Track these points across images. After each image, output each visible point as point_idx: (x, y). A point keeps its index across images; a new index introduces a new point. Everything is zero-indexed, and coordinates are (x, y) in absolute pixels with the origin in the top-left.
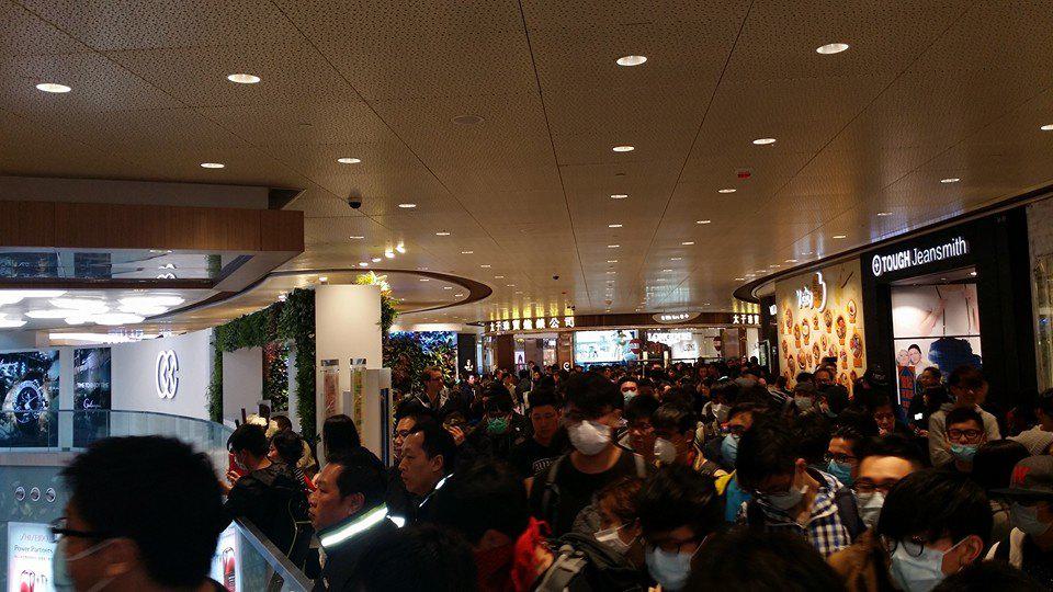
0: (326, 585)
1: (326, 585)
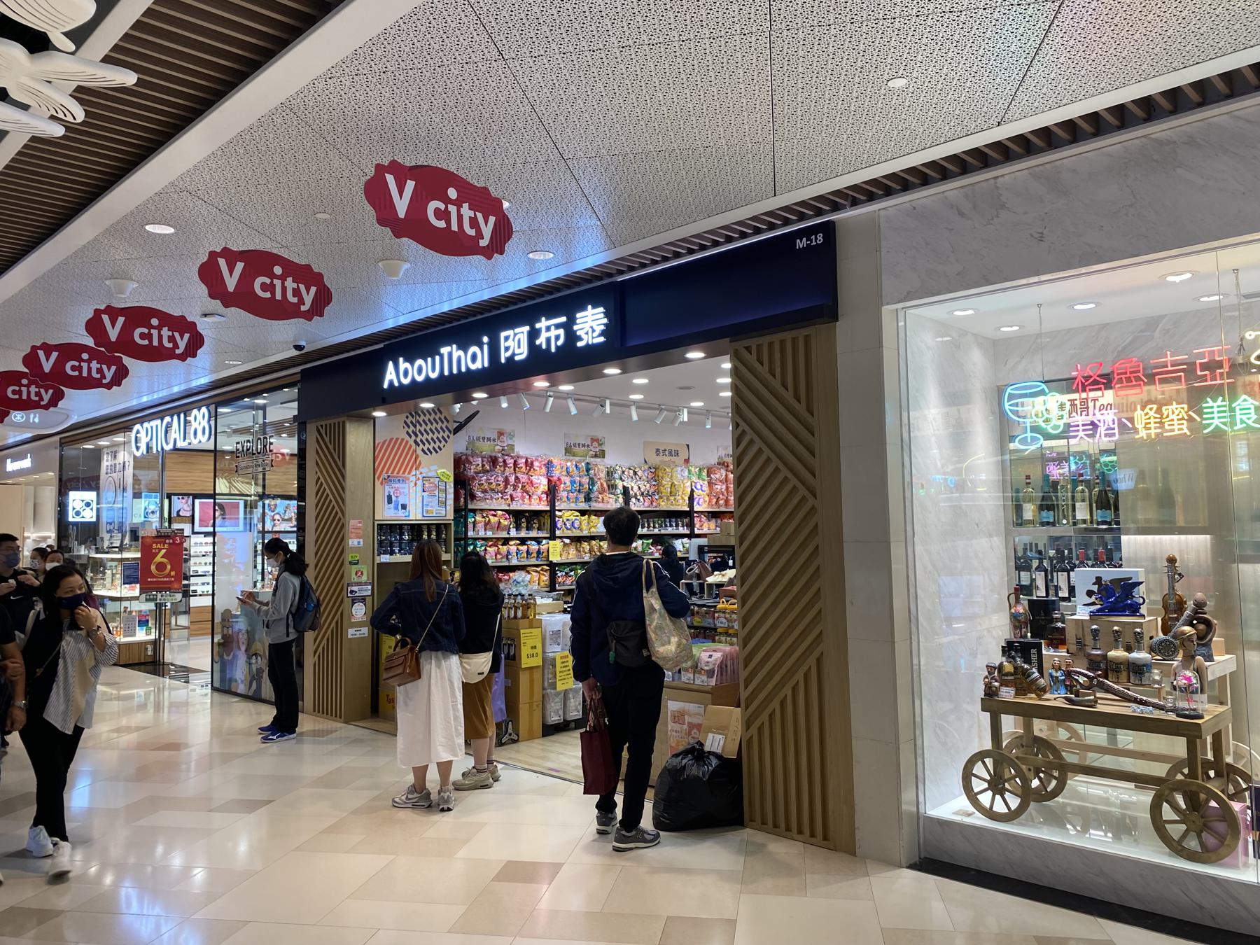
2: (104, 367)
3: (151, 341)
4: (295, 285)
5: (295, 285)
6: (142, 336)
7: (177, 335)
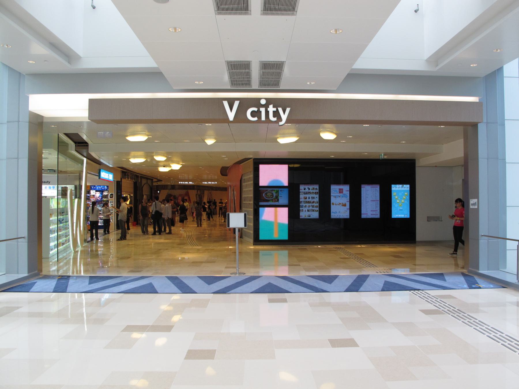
0: (31, 62)
1: (31, 62)
2: (280, 110)
3: (260, 117)
4: (275, 109)
5: (275, 109)
6: (253, 114)
7: (280, 110)
